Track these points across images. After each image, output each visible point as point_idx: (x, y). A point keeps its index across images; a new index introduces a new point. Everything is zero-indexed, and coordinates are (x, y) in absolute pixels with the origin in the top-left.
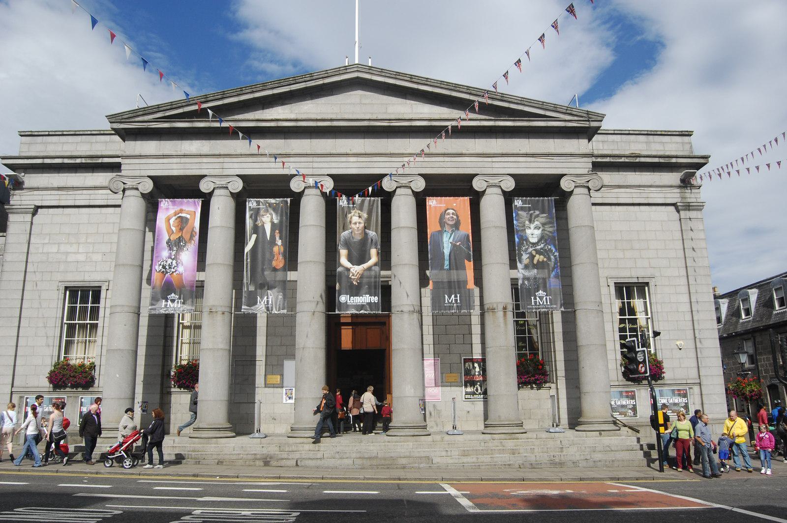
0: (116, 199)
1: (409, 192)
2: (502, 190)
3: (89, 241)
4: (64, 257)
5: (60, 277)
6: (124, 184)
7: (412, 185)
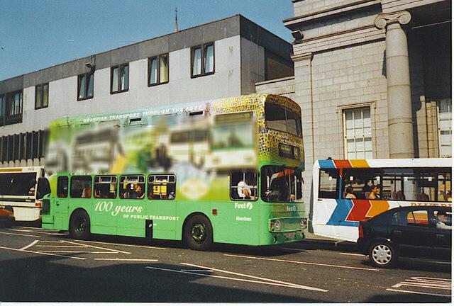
0: (379, 34)
1: (398, 25)
2: (400, 24)
3: (355, 72)
4: (338, 87)
5: (337, 103)
6: (387, 20)
7: (400, 20)
